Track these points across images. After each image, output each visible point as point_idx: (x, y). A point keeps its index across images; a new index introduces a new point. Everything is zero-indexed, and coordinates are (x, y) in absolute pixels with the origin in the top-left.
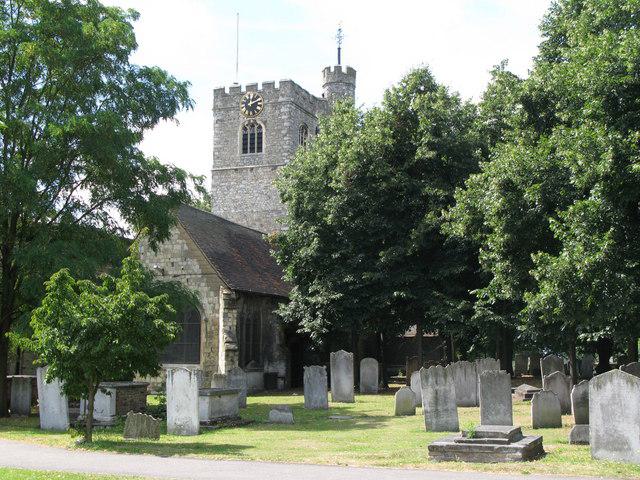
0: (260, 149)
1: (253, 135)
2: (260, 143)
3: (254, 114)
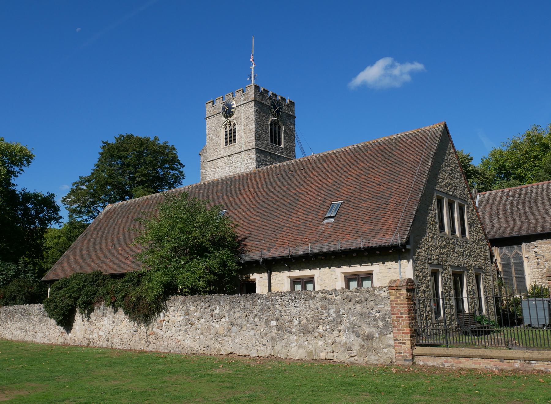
1: (275, 131)
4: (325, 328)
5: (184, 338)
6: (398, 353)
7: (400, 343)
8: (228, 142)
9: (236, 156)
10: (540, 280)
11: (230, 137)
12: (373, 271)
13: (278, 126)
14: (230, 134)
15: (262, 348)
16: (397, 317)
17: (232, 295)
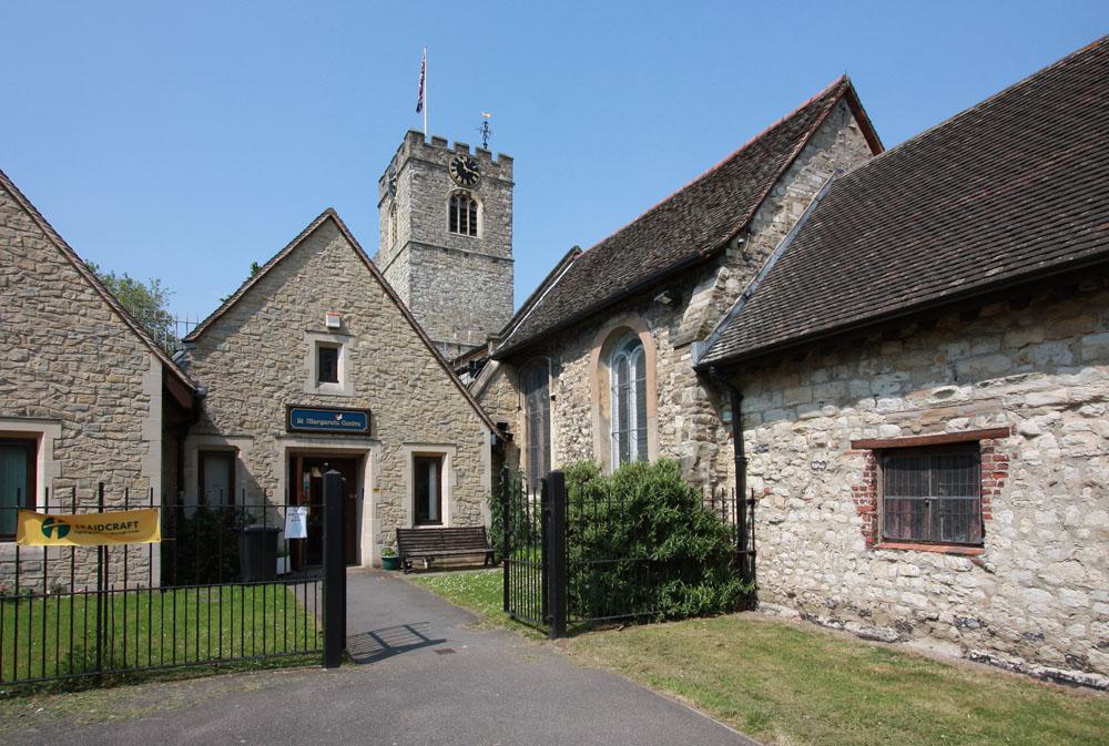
0: (473, 232)
2: (474, 225)
3: (468, 183)
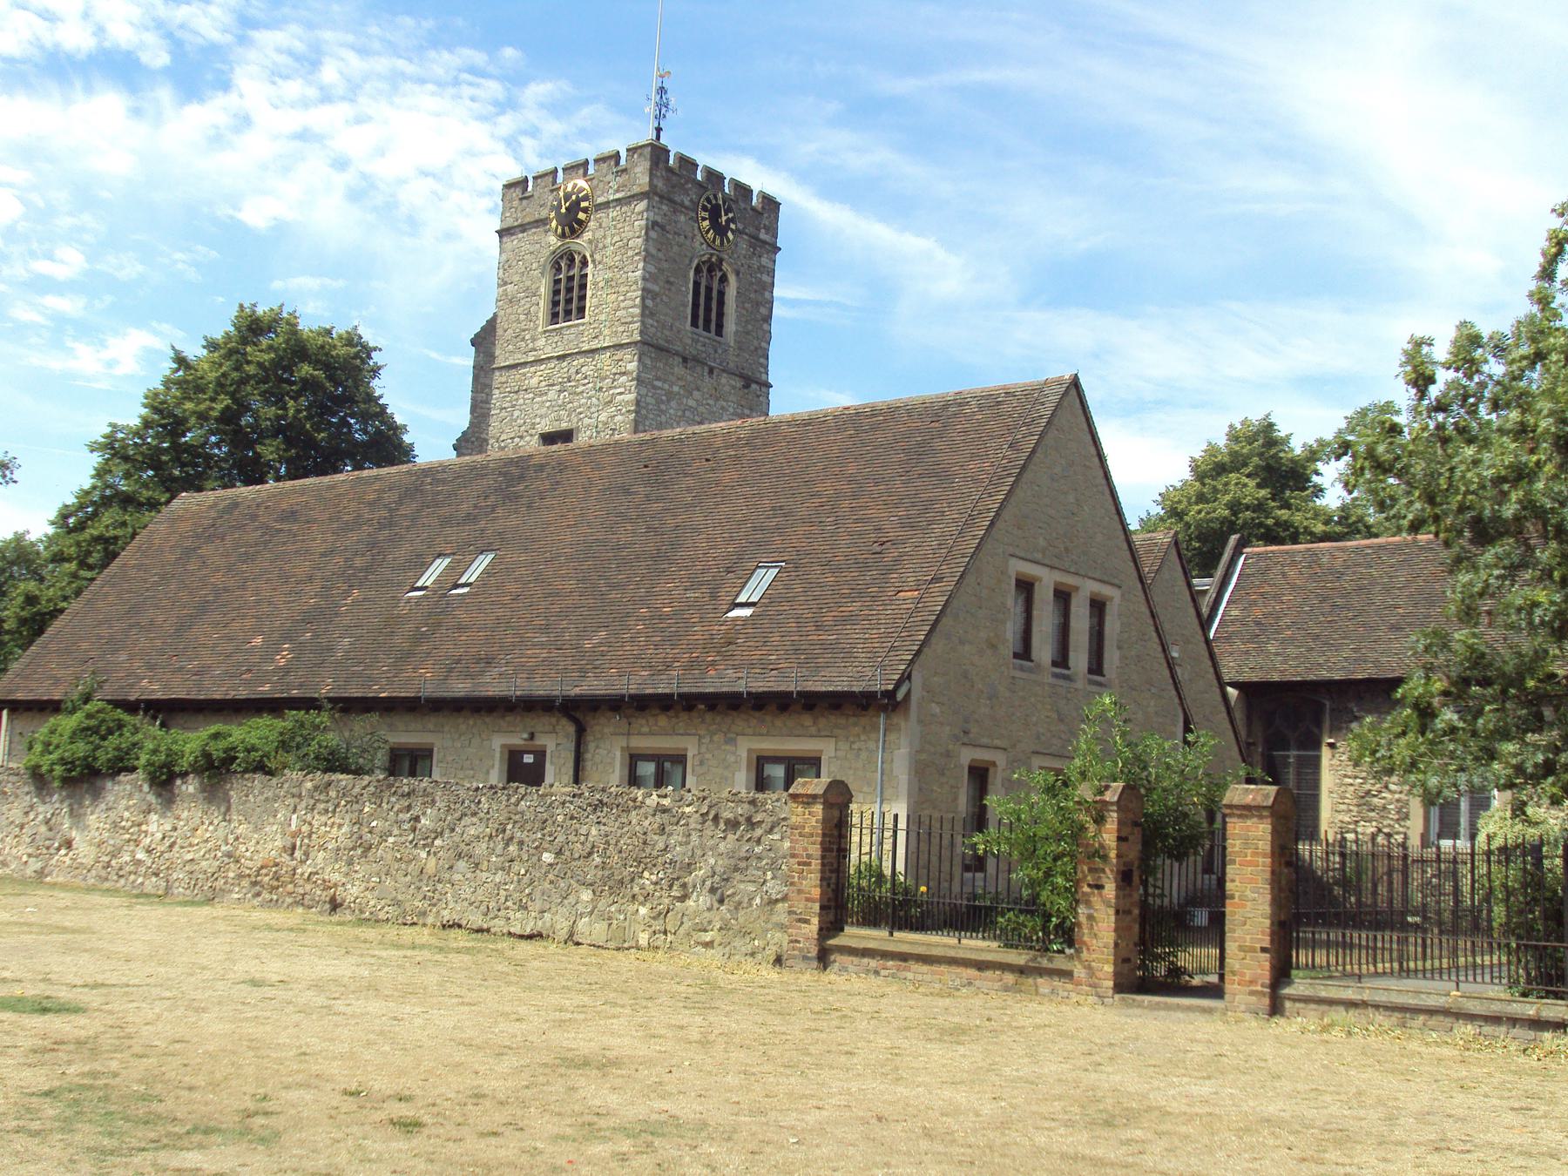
0: (719, 332)
1: (709, 289)
4: (654, 878)
5: (344, 880)
6: (792, 941)
7: (800, 920)
8: (561, 314)
9: (582, 361)
10: (1355, 809)
11: (569, 301)
12: (821, 751)
13: (719, 274)
14: (569, 290)
15: (518, 915)
16: (799, 864)
17: (843, 782)
